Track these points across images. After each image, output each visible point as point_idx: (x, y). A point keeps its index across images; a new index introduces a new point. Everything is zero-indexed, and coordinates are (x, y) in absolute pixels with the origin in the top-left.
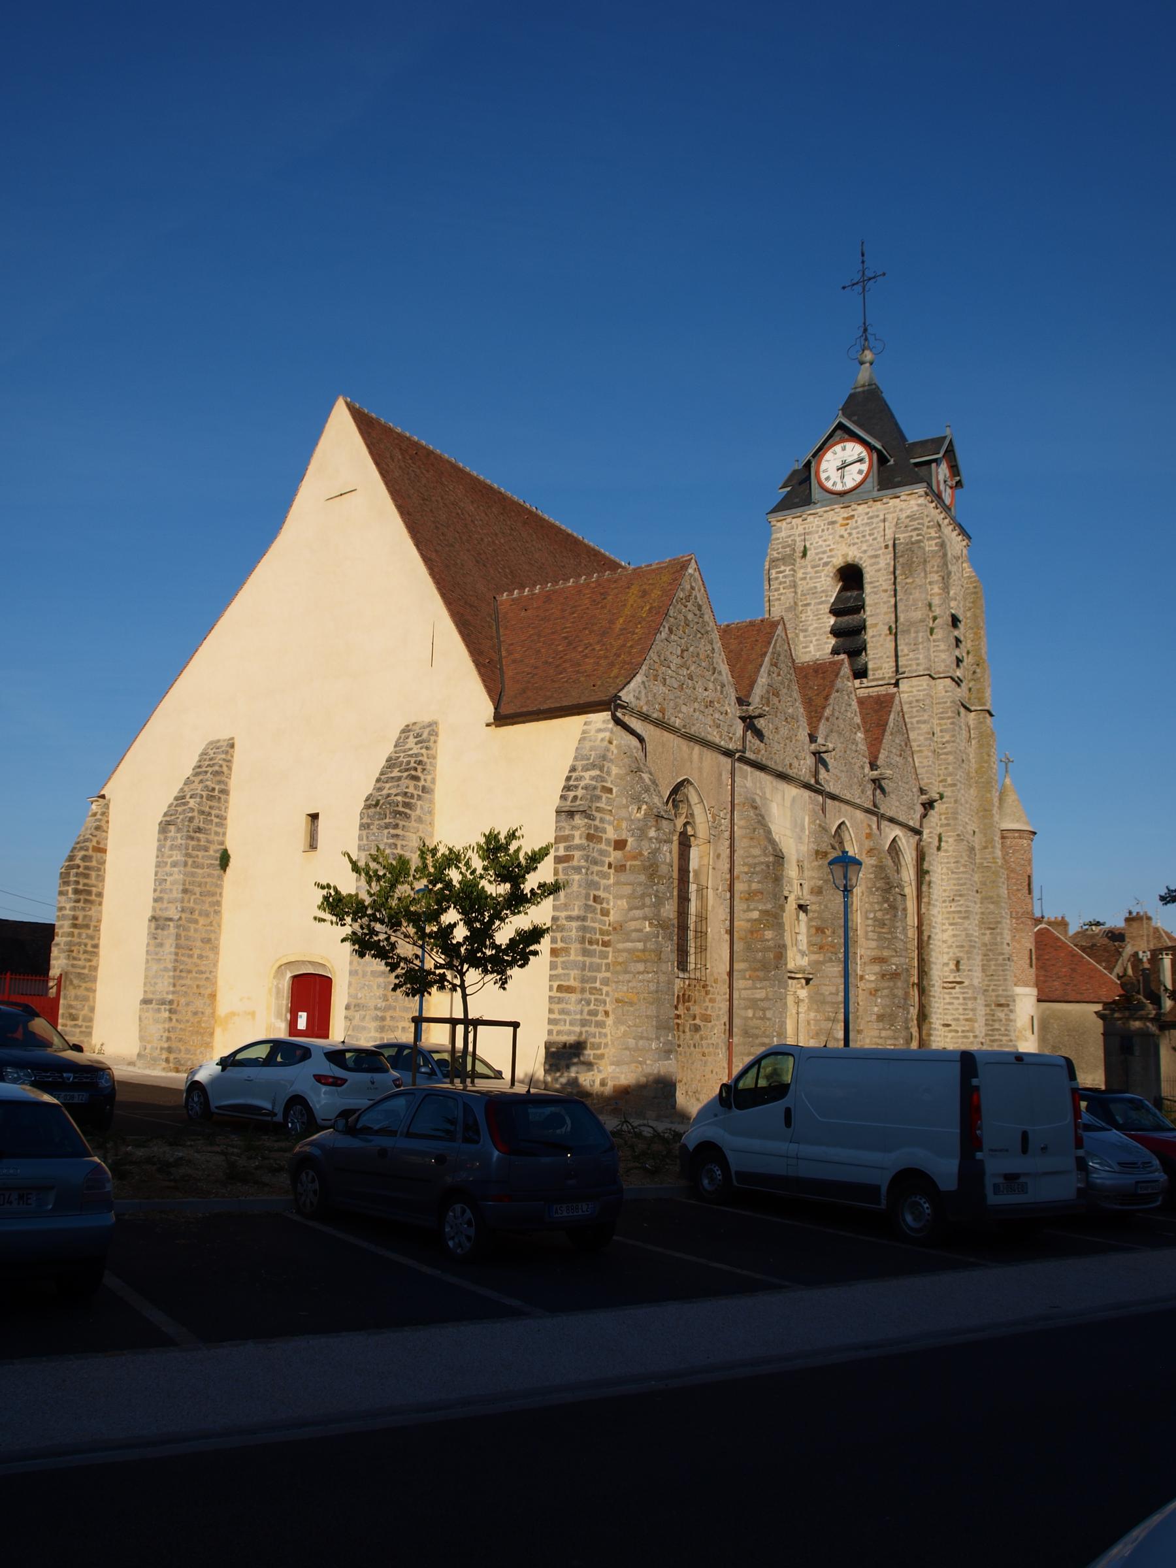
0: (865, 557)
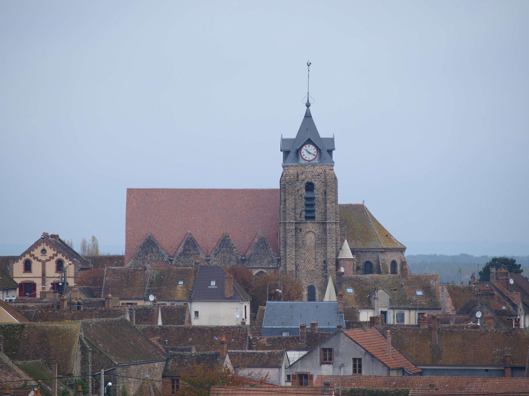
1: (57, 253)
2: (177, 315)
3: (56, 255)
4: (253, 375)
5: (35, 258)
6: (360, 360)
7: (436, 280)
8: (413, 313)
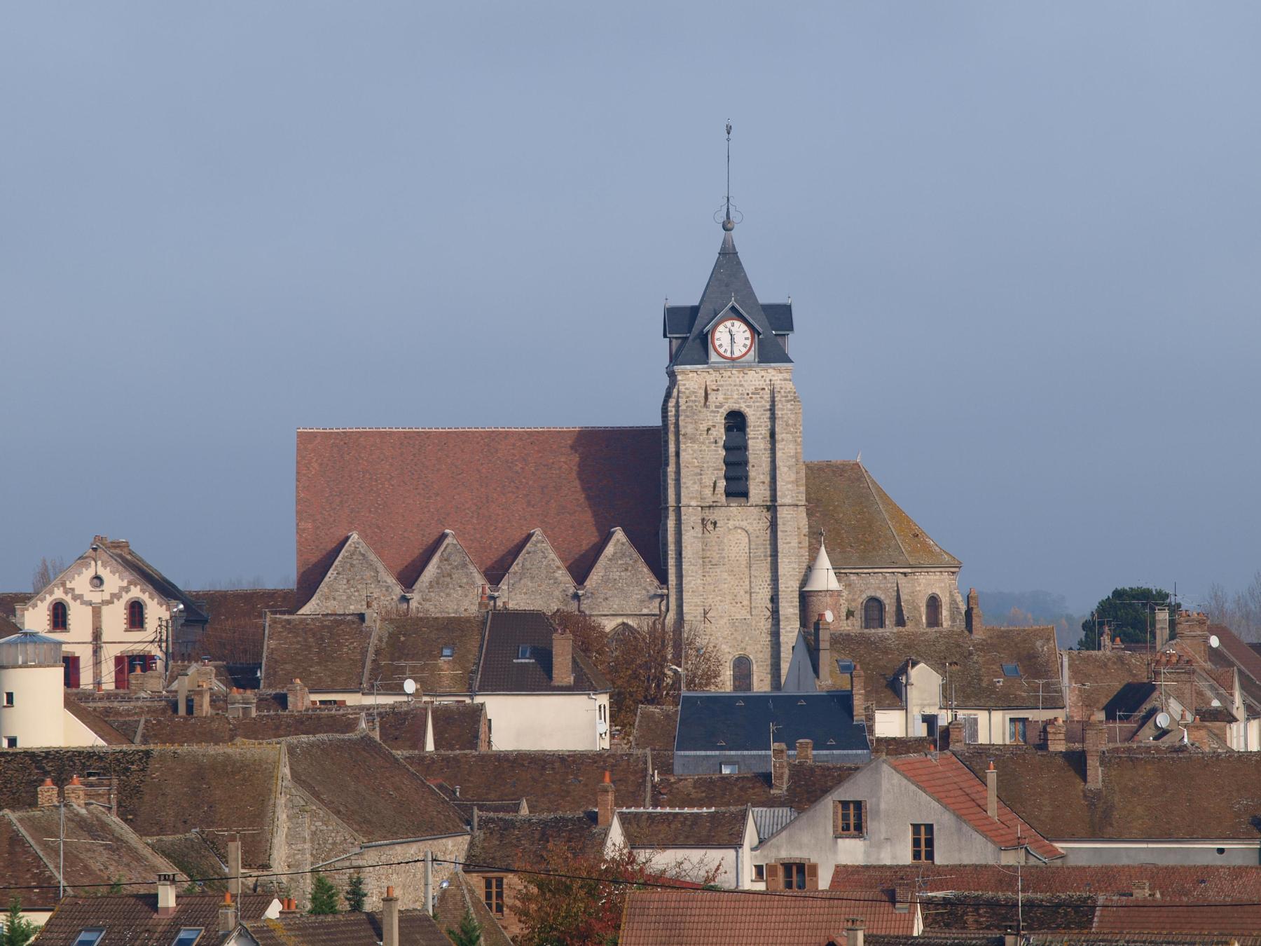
0: (743, 405)
1: (130, 583)
2: (468, 725)
3: (127, 590)
6: (930, 828)
7: (1048, 640)
8: (998, 716)
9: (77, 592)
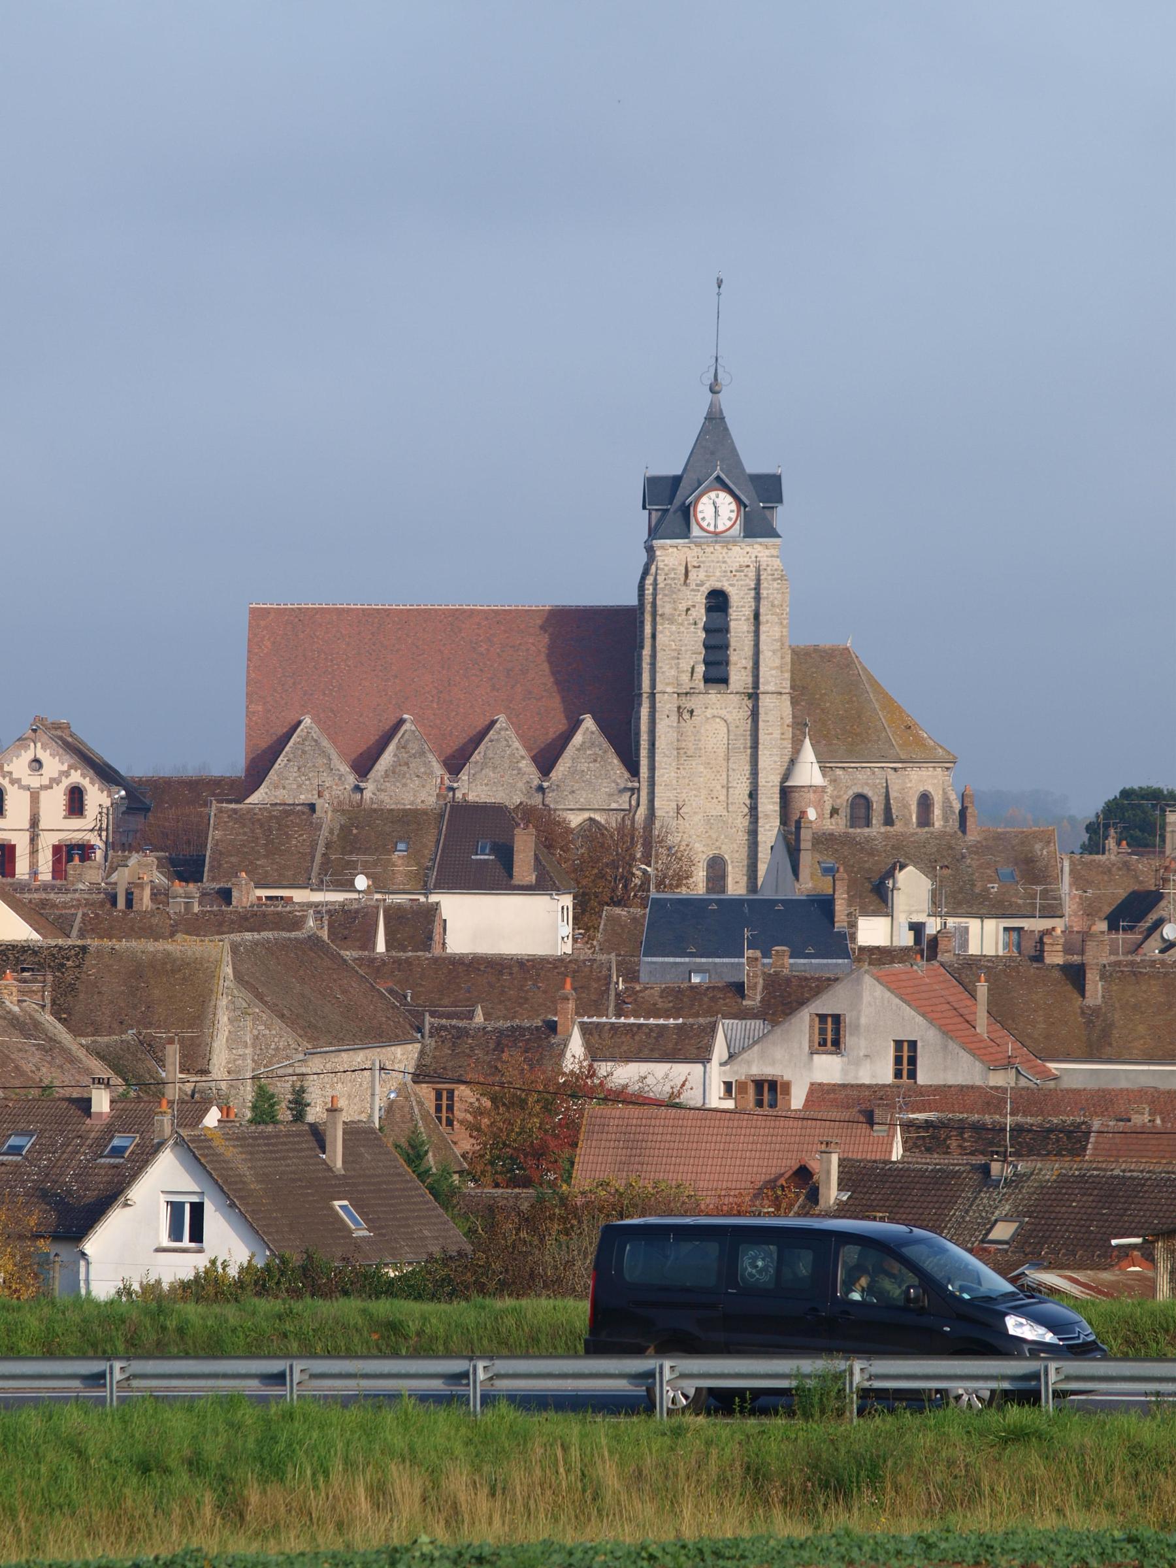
1: (70, 767)
2: (419, 926)
3: (67, 774)
4: (649, 1081)
5: (13, 782)
6: (913, 1045)
7: (1049, 842)
8: (991, 925)
9: (15, 776)
